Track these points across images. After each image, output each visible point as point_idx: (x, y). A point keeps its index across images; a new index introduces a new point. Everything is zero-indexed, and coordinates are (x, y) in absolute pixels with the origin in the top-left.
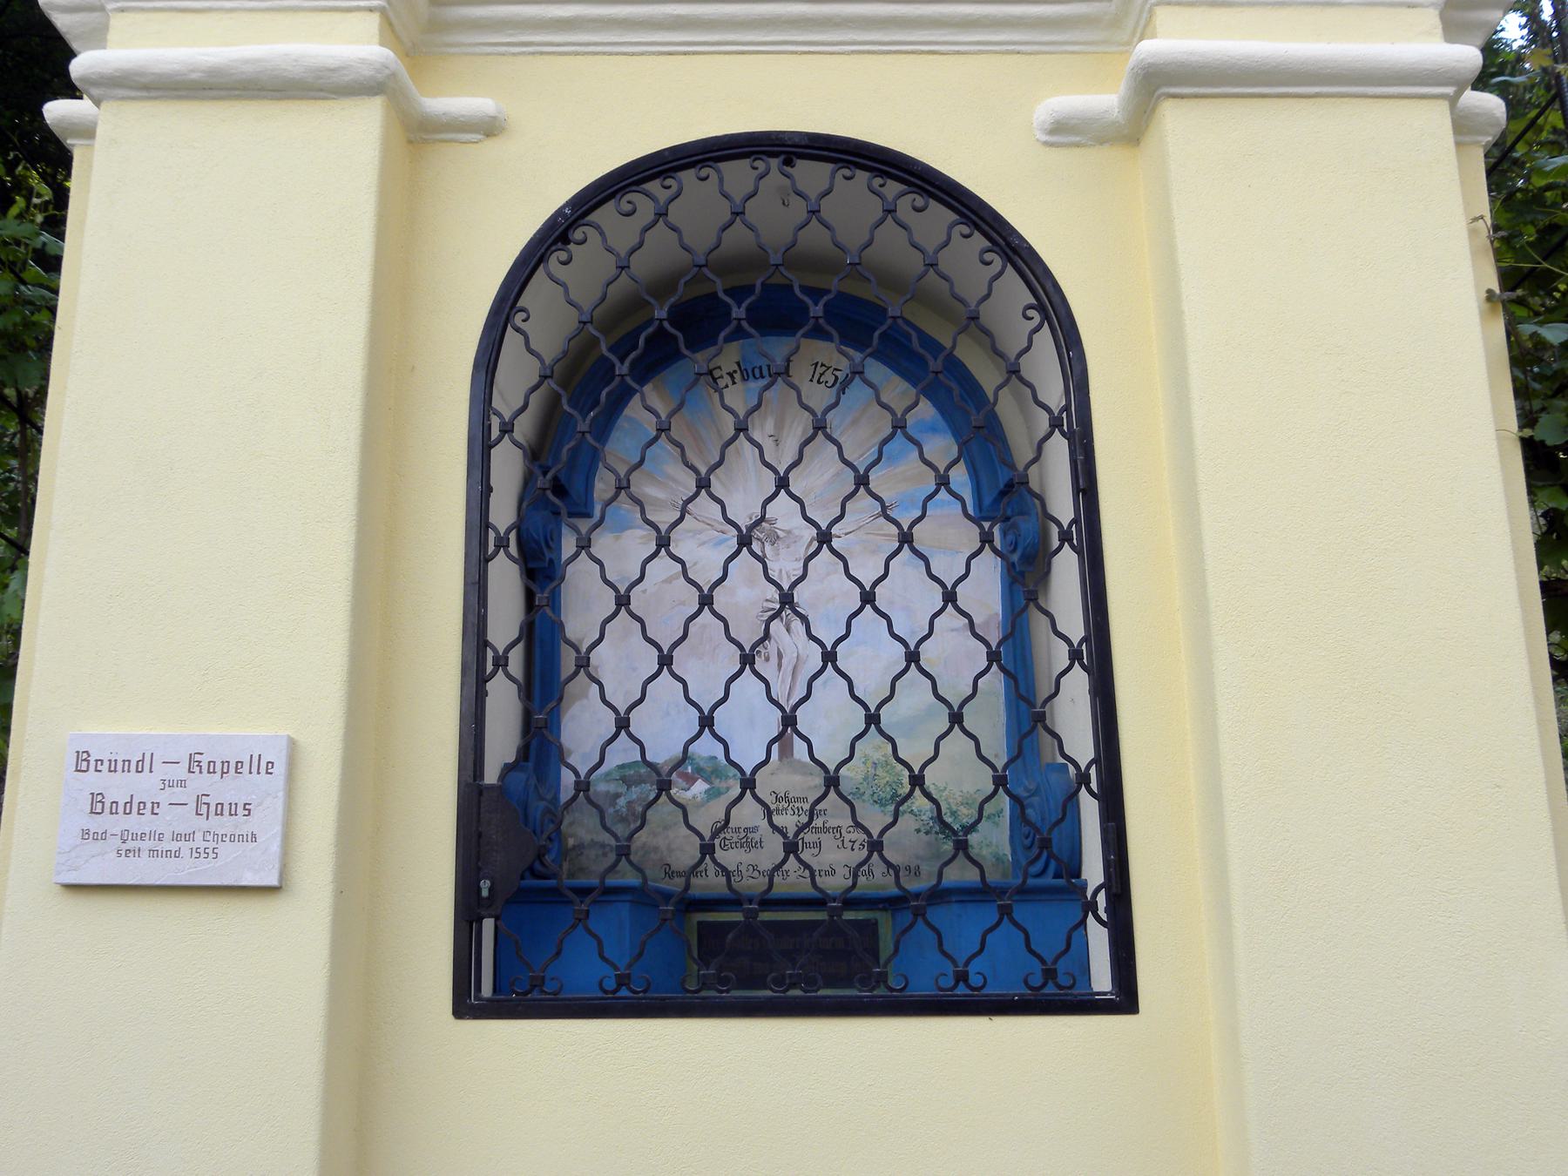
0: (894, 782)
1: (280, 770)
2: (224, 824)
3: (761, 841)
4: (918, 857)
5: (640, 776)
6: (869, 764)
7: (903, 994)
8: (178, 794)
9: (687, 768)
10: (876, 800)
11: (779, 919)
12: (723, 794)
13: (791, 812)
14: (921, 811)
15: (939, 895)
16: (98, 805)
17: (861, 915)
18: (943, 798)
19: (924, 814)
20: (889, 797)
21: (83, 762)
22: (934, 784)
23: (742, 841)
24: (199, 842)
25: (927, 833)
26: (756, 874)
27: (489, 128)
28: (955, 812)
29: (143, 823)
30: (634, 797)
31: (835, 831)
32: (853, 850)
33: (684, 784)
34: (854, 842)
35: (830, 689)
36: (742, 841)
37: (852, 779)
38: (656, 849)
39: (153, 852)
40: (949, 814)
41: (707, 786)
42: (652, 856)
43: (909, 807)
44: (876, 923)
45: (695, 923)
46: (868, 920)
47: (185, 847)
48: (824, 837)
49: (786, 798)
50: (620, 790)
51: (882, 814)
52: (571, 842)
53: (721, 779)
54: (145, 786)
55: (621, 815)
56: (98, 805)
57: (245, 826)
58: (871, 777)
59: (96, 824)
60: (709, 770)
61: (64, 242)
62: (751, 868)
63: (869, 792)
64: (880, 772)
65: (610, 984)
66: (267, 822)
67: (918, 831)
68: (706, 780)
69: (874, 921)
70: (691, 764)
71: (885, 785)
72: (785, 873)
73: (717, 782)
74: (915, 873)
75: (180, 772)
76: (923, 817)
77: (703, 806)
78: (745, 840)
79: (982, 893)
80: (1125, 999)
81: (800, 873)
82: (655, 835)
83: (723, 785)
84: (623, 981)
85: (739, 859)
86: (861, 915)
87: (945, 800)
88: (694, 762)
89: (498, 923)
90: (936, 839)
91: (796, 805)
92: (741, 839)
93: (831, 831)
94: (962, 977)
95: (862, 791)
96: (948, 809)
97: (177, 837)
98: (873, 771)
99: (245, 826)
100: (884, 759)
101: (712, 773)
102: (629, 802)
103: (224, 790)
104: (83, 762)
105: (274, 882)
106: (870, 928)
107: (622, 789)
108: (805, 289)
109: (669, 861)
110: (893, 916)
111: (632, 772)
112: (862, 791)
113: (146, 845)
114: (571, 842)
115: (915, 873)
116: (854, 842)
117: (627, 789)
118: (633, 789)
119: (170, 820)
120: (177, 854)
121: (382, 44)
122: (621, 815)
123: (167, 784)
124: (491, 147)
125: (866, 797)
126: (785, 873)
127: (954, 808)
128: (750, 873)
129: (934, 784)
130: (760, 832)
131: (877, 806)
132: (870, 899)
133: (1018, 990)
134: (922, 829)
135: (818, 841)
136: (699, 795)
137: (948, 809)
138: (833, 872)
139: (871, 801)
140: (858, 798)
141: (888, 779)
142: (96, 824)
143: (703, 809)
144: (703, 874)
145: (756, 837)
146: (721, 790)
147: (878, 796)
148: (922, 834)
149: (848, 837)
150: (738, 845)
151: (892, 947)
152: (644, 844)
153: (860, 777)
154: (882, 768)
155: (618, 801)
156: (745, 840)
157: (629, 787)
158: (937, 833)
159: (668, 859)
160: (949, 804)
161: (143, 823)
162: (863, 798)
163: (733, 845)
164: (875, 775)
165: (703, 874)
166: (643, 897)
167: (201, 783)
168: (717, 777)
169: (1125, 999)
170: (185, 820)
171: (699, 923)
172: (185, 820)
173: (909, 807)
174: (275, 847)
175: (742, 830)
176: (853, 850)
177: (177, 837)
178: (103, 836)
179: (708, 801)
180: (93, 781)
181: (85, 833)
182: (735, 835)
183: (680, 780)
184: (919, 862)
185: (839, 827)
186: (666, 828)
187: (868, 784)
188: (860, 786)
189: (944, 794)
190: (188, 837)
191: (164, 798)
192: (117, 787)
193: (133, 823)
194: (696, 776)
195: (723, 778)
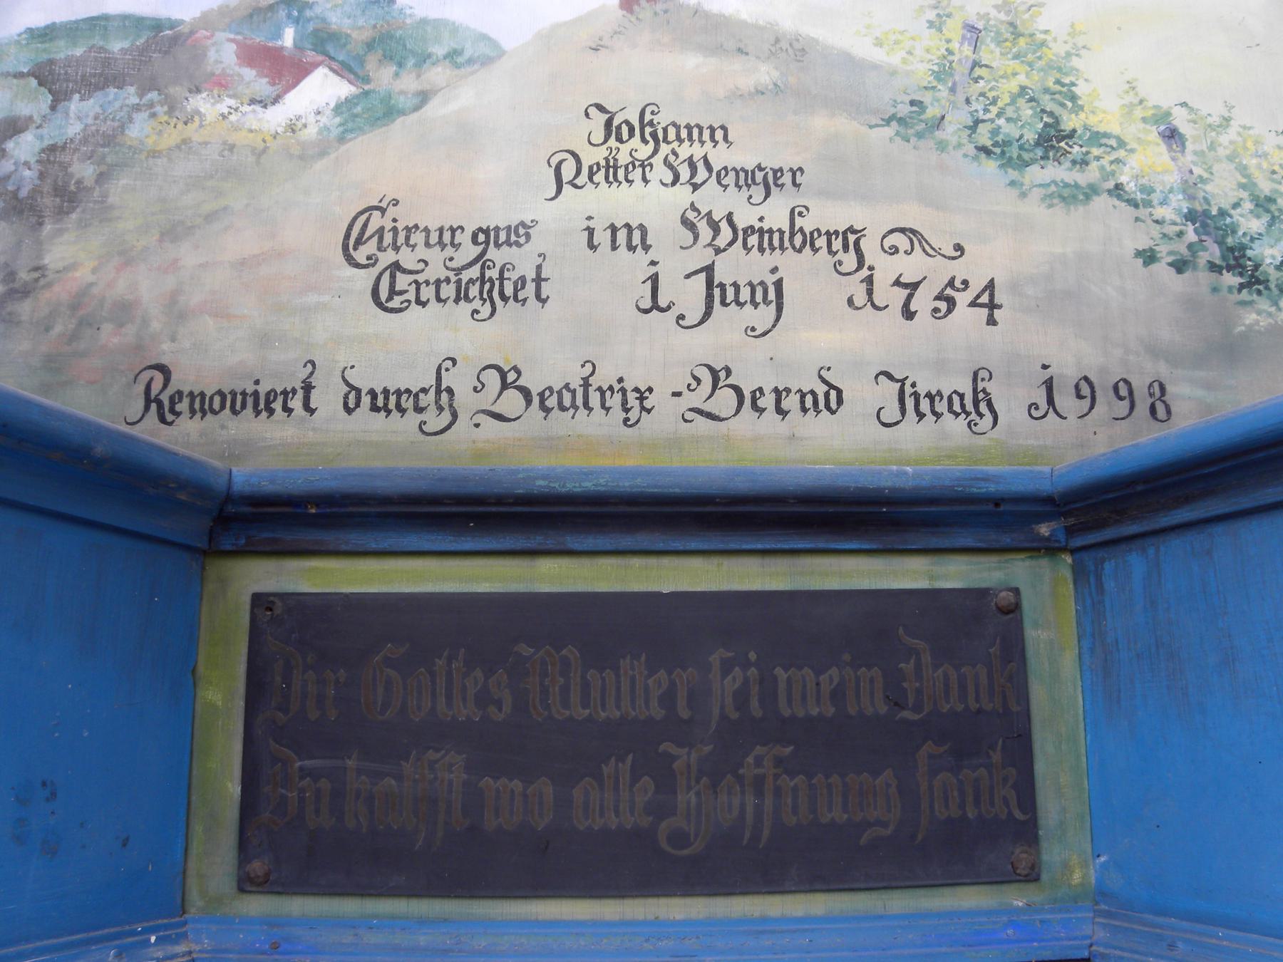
0: (1046, 90)
3: (539, 280)
4: (1154, 351)
5: (107, 62)
6: (954, 29)
7: (481, 263)
9: (278, 35)
10: (989, 143)
11: (603, 587)
12: (402, 113)
13: (660, 172)
14: (1149, 190)
18: (1221, 152)
19: (1164, 203)
20: (1030, 136)
22: (1184, 104)
23: (465, 276)
25: (1180, 266)
26: (511, 402)
28: (1271, 200)
30: (74, 129)
31: (837, 244)
32: (909, 314)
33: (262, 86)
34: (915, 286)
36: (465, 276)
37: (893, 73)
38: (124, 311)
40: (1248, 206)
41: (342, 89)
42: (109, 336)
43: (1106, 176)
44: (1013, 610)
45: (246, 601)
46: (982, 594)
48: (793, 266)
49: (646, 127)
50: (24, 109)
51: (1014, 192)
53: (400, 65)
55: (15, 194)
58: (961, 71)
60: (366, 35)
61: (262, 107)
62: (492, 379)
63: (957, 119)
64: (990, 53)
67: (1149, 257)
68: (345, 70)
69: (1006, 597)
70: (297, 21)
71: (1013, 101)
72: (632, 397)
73: (384, 77)
74: (1153, 410)
76: (1160, 212)
77: (323, 154)
78: (474, 272)
81: (696, 399)
82: (127, 258)
83: (409, 83)
85: (444, 348)
87: (1231, 158)
88: (308, 13)
89: (255, 610)
90: (1215, 290)
91: (685, 151)
92: (458, 271)
93: (821, 242)
95: (932, 112)
96: (1243, 187)
98: (967, 50)
100: (1002, 16)
101: (370, 46)
102: (52, 149)
107: (34, 104)
108: (830, 685)
109: (166, 352)
110: (1079, 574)
111: (78, 52)
112: (932, 112)
115: (1153, 410)
116: (915, 286)
117: (53, 108)
118: (75, 105)
122: (15, 194)
125: (950, 131)
126: (632, 397)
127: (1265, 187)
128: (486, 399)
129: (1184, 104)
130: (538, 243)
131: (991, 166)
132: (998, 501)
134: (1163, 249)
135: (770, 280)
136: (311, 119)
137: (1243, 187)
139: (970, 149)
140: (920, 135)
141: (1022, 79)
143: (319, 165)
144: (296, 403)
145: (522, 261)
146: (401, 102)
147: (995, 132)
148: (1162, 269)
149: (886, 269)
150: (448, 291)
151: (161, 386)
152: (85, 291)
153: (921, 70)
154: (999, 43)
155: (10, 145)
156: (474, 272)
157: (59, 98)
158: (1213, 267)
159: (166, 346)
160: (1243, 169)
162: (939, 134)
163: (428, 293)
164: (976, 64)
165: (296, 403)
168: (388, 57)
171: (261, 602)
173: (1106, 176)
175: (464, 238)
176: (909, 314)
179: (341, 140)
182: (436, 257)
183: (249, 73)
184: (1163, 370)
185: (851, 230)
186: (173, 232)
187: (953, 90)
188: (927, 98)
189: (1224, 139)
194: (311, 56)
195: (411, 62)
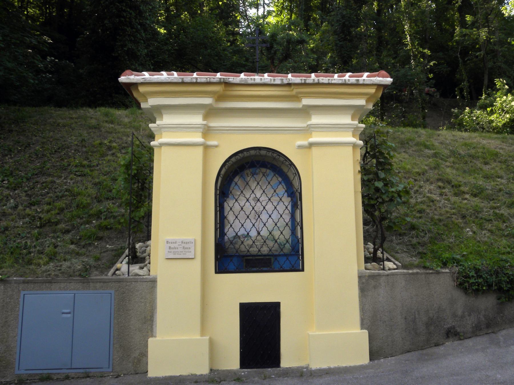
1: (194, 243)
2: (187, 250)
8: (180, 246)
15: (279, 255)
16: (170, 248)
17: (269, 257)
21: (167, 242)
24: (184, 253)
27: (216, 146)
29: (176, 250)
35: (264, 220)
39: (178, 254)
47: (182, 253)
52: (143, 15)
54: (176, 245)
56: (170, 248)
57: (190, 250)
59: (170, 250)
65: (235, 269)
66: (192, 250)
75: (181, 243)
79: (285, 255)
80: (303, 270)
84: (237, 269)
86: (269, 257)
94: (281, 267)
97: (181, 252)
99: (190, 250)
103: (186, 246)
104: (167, 242)
105: (193, 257)
106: (270, 259)
113: (177, 253)
114: (143, 15)
119: (180, 250)
120: (181, 254)
121: (202, 138)
123: (179, 245)
124: (216, 149)
133: (288, 269)
138: (265, 251)
142: (170, 250)
161: (176, 250)
166: (239, 256)
167: (183, 245)
169: (303, 270)
170: (181, 250)
171: (246, 259)
172: (181, 250)
174: (194, 253)
177: (181, 252)
178: (171, 252)
180: (169, 245)
181: (169, 252)
190: (182, 252)
191: (179, 247)
192: (172, 246)
193: (175, 250)
